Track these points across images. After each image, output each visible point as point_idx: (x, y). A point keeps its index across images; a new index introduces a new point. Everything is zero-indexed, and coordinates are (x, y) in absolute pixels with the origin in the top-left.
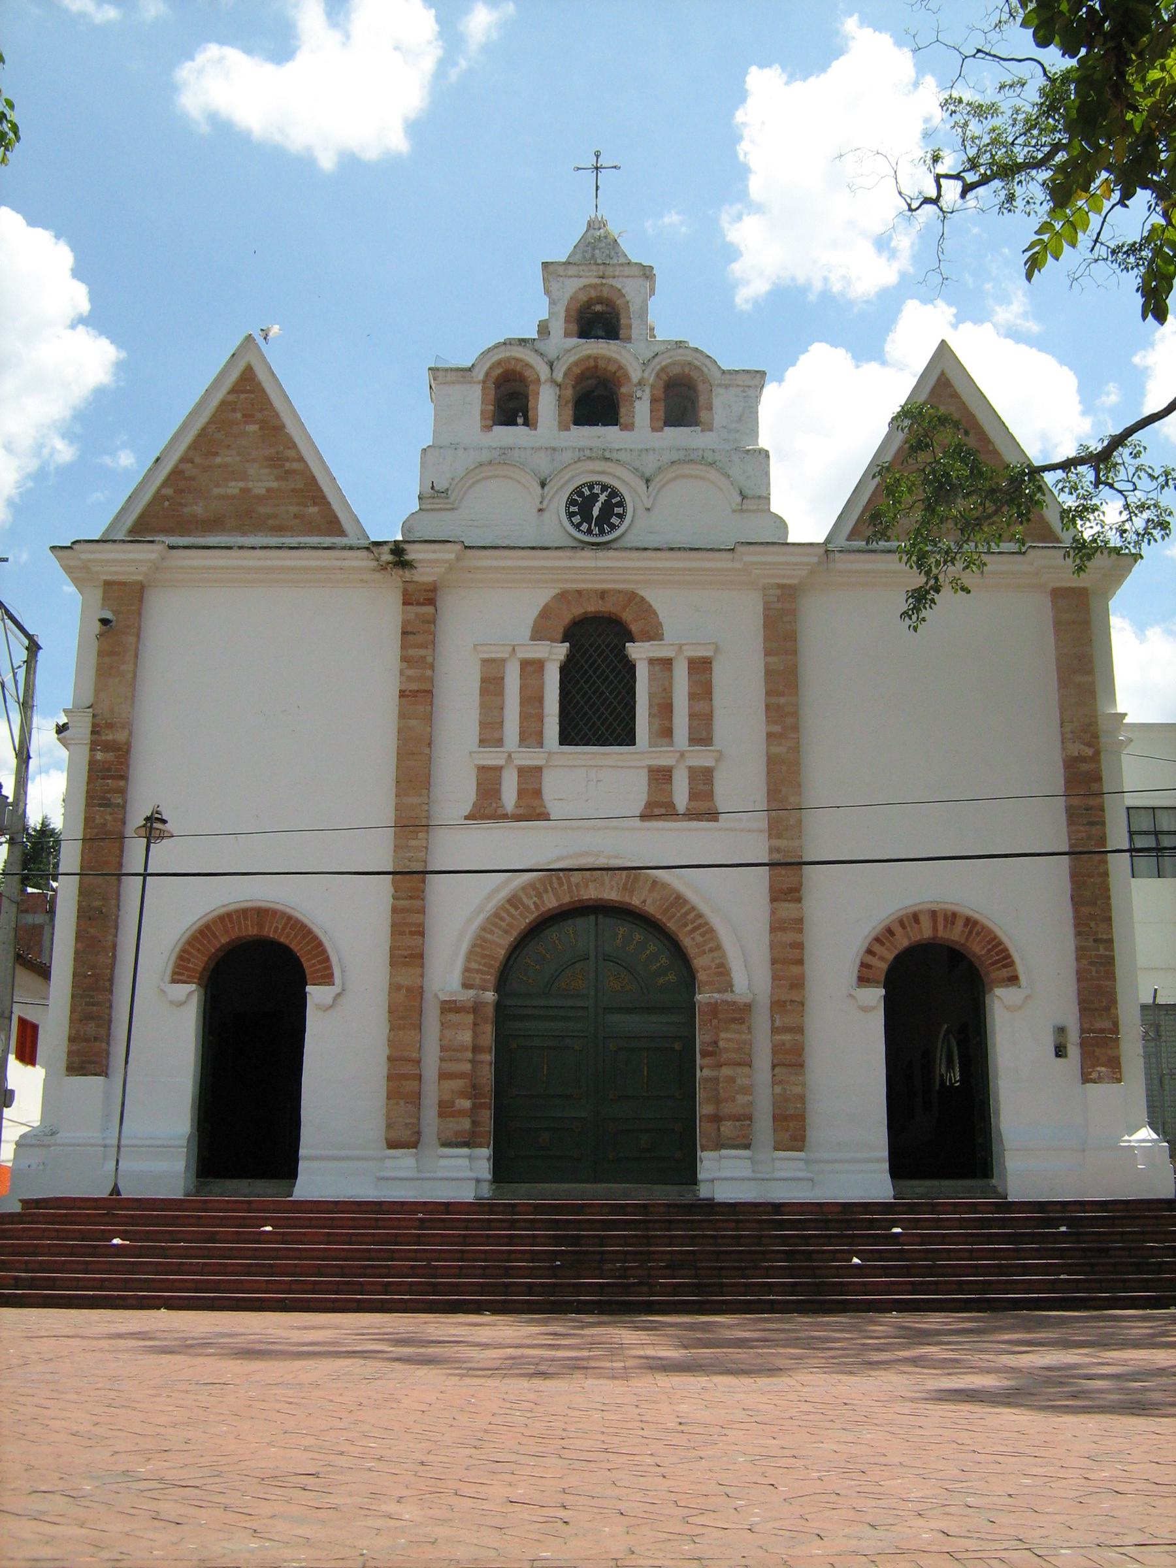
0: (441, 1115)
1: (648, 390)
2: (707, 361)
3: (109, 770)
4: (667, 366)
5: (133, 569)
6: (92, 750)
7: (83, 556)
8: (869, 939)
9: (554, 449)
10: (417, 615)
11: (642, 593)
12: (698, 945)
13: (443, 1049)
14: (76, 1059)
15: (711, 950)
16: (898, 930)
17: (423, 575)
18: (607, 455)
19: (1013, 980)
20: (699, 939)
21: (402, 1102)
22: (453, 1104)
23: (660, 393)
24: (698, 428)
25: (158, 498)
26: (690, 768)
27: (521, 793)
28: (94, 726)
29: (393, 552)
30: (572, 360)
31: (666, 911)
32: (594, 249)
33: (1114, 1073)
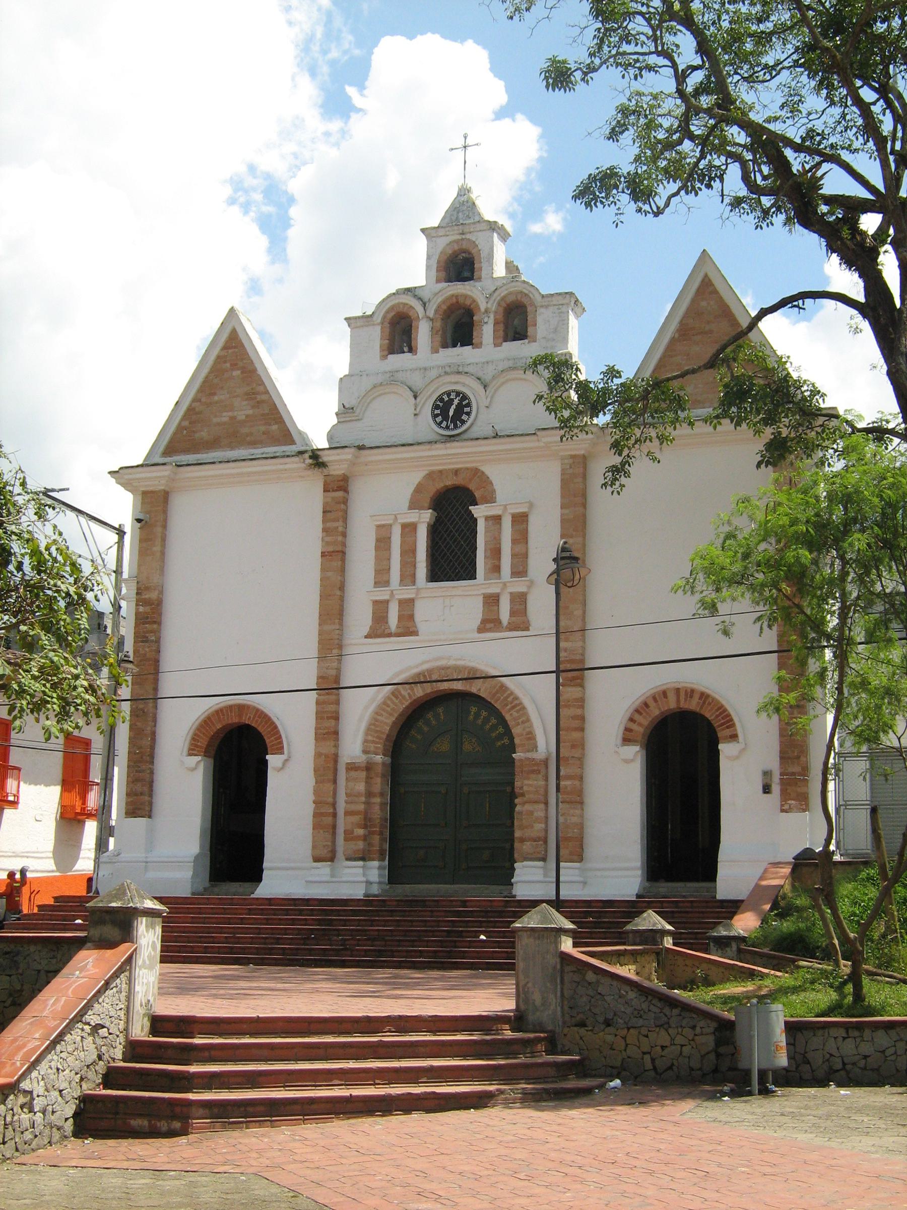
0: (346, 840)
1: (492, 316)
2: (531, 289)
3: (147, 618)
4: (505, 297)
5: (156, 482)
6: (137, 605)
7: (126, 477)
8: (631, 710)
9: (425, 369)
10: (333, 498)
11: (483, 469)
12: (515, 719)
13: (347, 795)
14: (131, 807)
15: (523, 722)
16: (652, 704)
17: (336, 470)
18: (461, 369)
19: (734, 737)
20: (515, 714)
21: (321, 831)
22: (352, 832)
23: (500, 317)
24: (526, 341)
25: (180, 428)
26: (511, 593)
27: (400, 618)
28: (138, 589)
29: (311, 457)
30: (440, 300)
31: (494, 695)
32: (458, 213)
33: (802, 805)
